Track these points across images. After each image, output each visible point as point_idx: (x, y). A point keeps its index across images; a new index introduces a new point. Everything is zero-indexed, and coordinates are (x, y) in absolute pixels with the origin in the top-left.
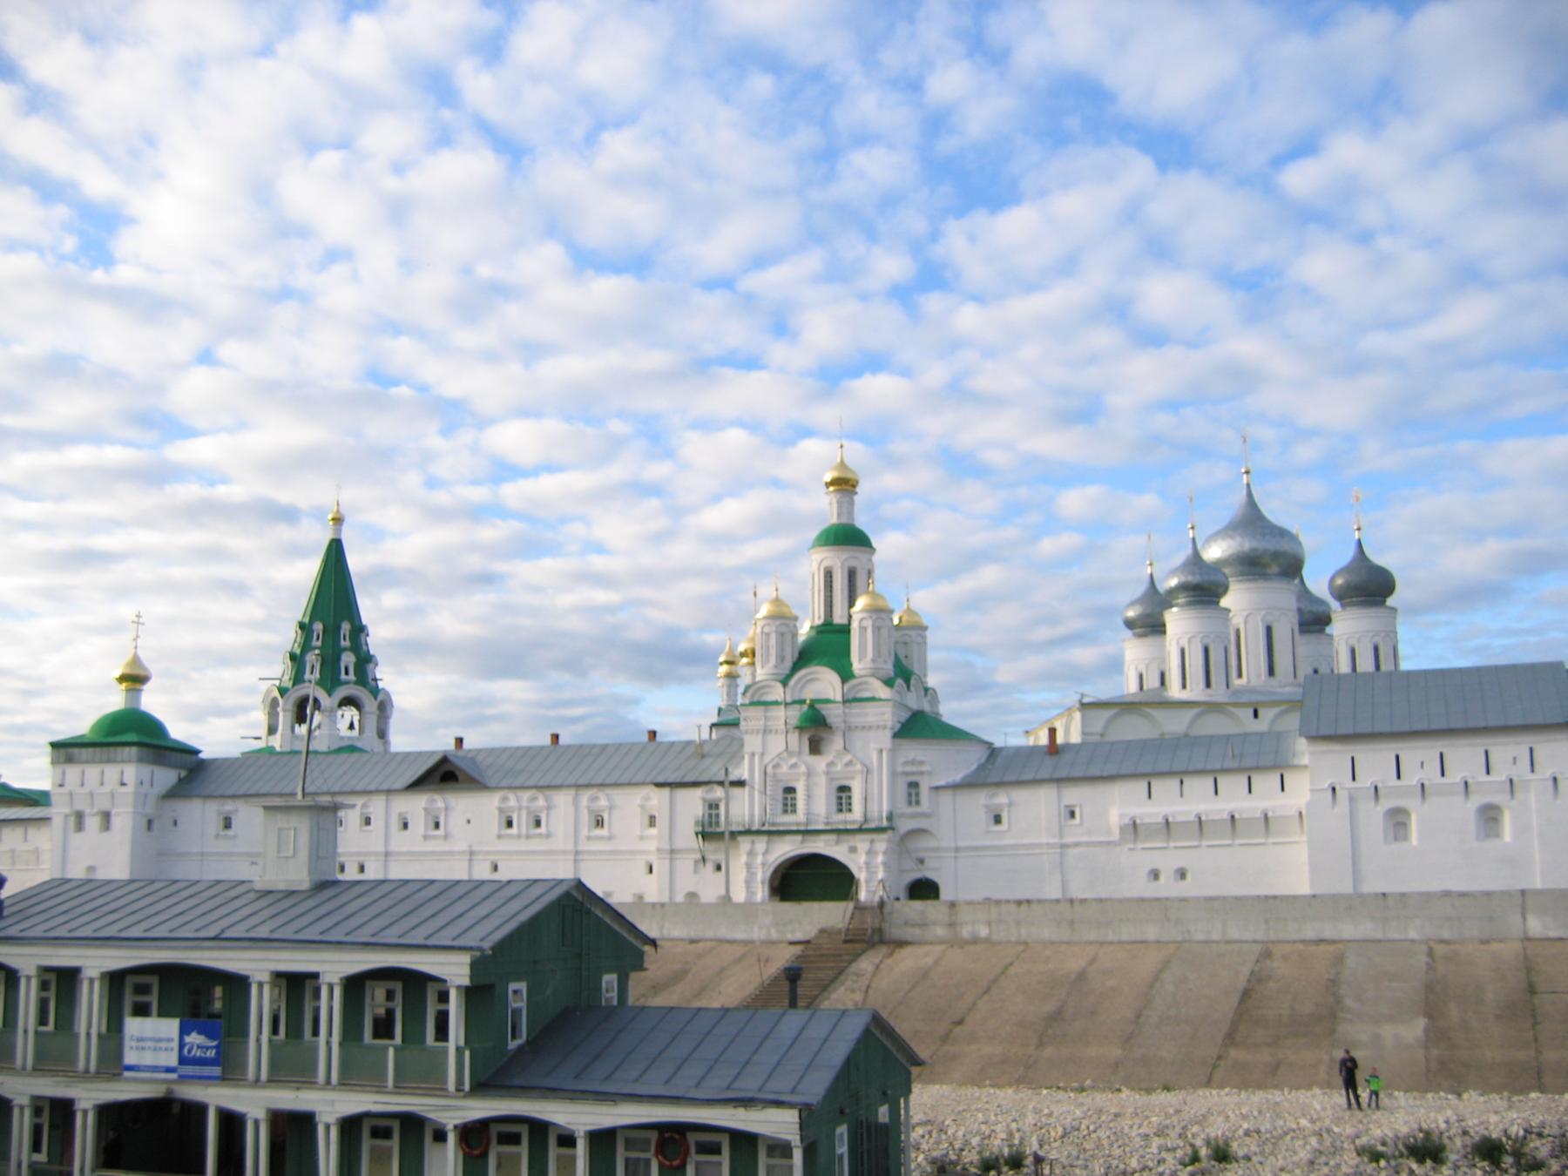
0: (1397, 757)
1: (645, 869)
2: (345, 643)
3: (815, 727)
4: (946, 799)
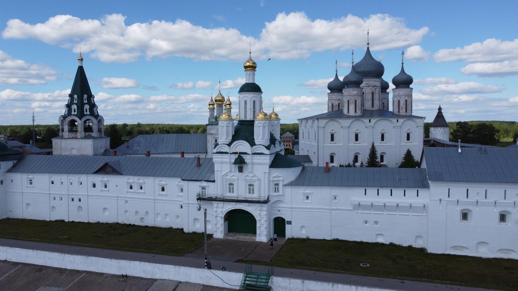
0: (467, 190)
1: (179, 207)
2: (86, 102)
3: (240, 162)
4: (288, 190)
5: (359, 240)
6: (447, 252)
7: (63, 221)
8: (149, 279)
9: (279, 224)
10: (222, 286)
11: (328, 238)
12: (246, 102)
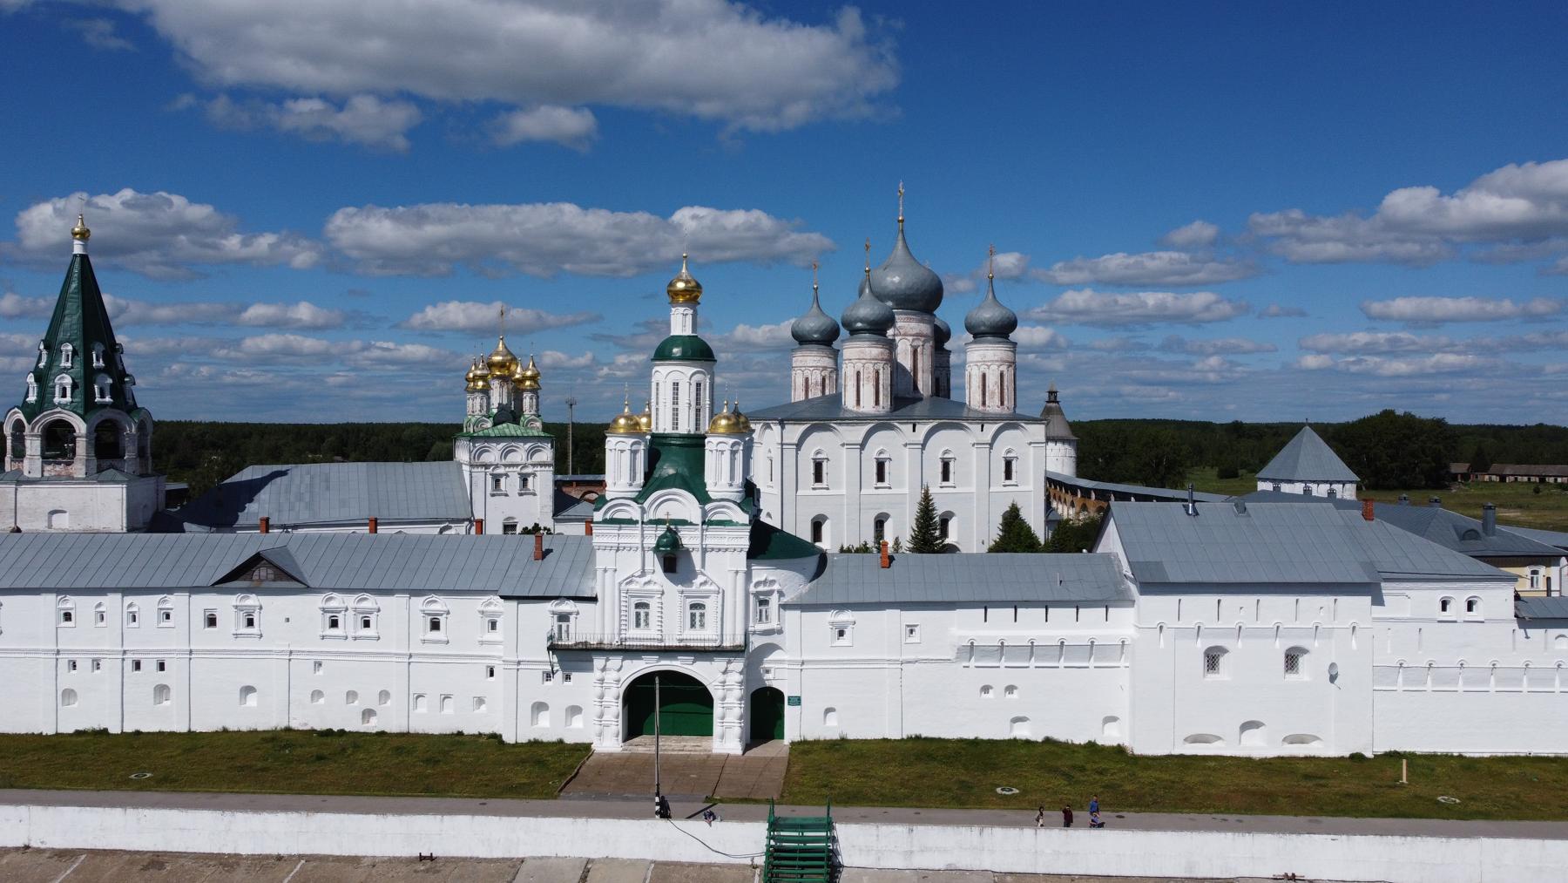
1: (485, 672)
4: (792, 616)
5: (972, 737)
6: (1176, 752)
7: (104, 732)
8: (497, 860)
9: (765, 710)
10: (704, 860)
11: (895, 734)
12: (676, 385)
